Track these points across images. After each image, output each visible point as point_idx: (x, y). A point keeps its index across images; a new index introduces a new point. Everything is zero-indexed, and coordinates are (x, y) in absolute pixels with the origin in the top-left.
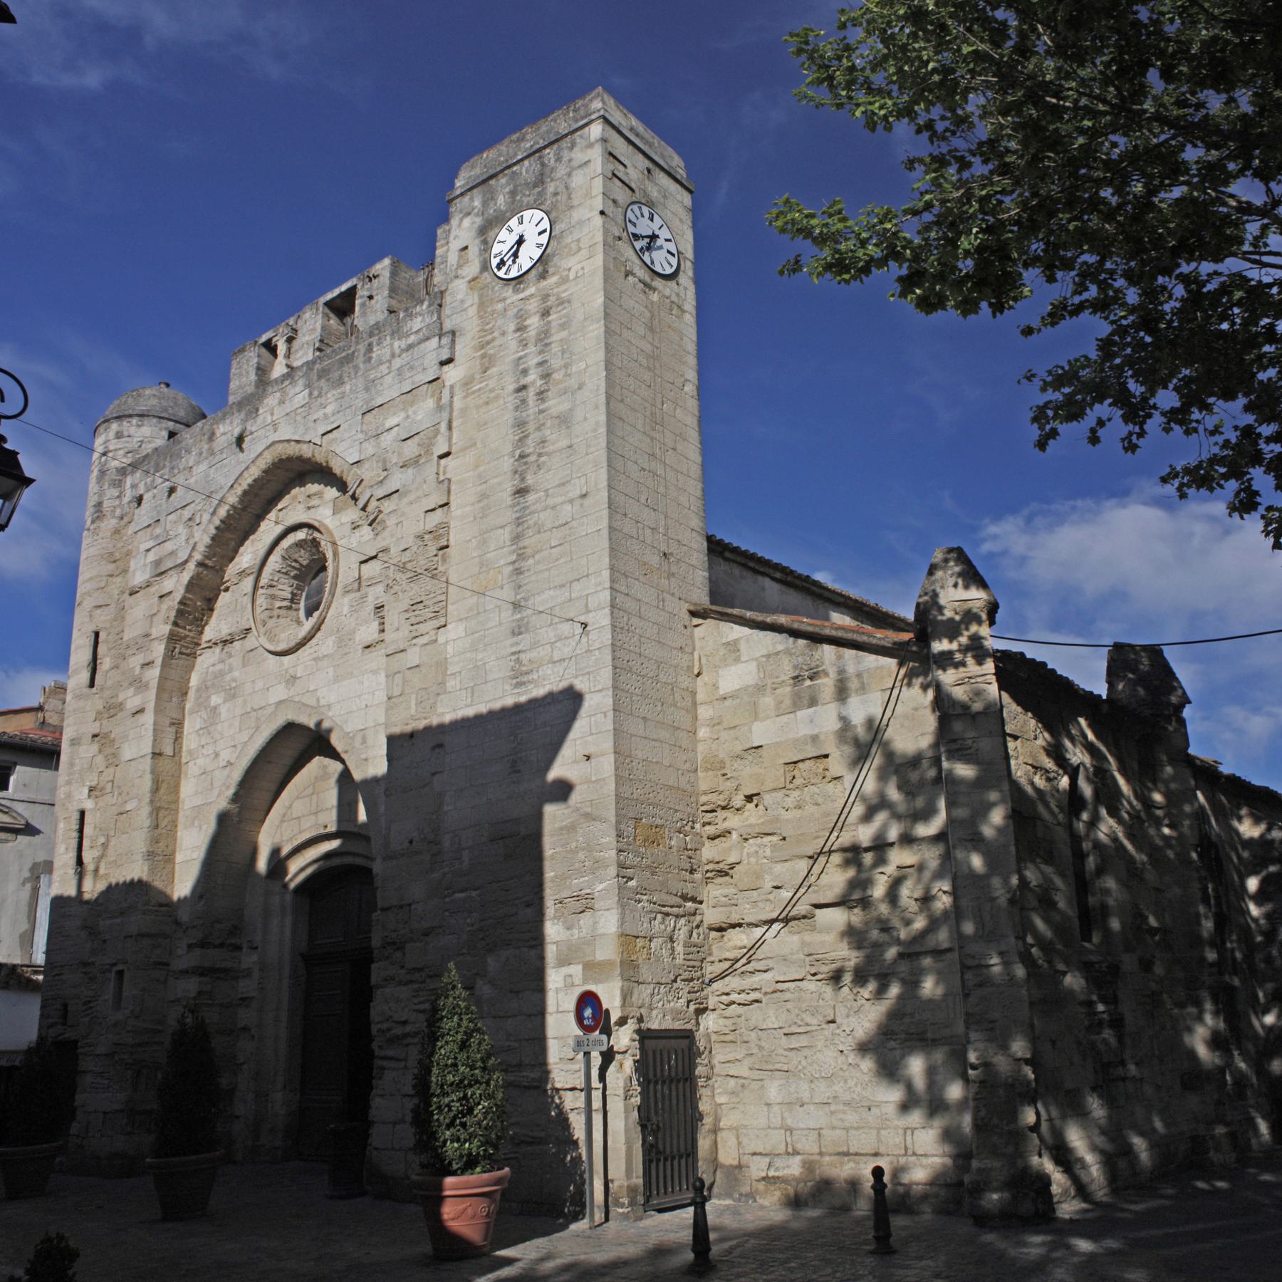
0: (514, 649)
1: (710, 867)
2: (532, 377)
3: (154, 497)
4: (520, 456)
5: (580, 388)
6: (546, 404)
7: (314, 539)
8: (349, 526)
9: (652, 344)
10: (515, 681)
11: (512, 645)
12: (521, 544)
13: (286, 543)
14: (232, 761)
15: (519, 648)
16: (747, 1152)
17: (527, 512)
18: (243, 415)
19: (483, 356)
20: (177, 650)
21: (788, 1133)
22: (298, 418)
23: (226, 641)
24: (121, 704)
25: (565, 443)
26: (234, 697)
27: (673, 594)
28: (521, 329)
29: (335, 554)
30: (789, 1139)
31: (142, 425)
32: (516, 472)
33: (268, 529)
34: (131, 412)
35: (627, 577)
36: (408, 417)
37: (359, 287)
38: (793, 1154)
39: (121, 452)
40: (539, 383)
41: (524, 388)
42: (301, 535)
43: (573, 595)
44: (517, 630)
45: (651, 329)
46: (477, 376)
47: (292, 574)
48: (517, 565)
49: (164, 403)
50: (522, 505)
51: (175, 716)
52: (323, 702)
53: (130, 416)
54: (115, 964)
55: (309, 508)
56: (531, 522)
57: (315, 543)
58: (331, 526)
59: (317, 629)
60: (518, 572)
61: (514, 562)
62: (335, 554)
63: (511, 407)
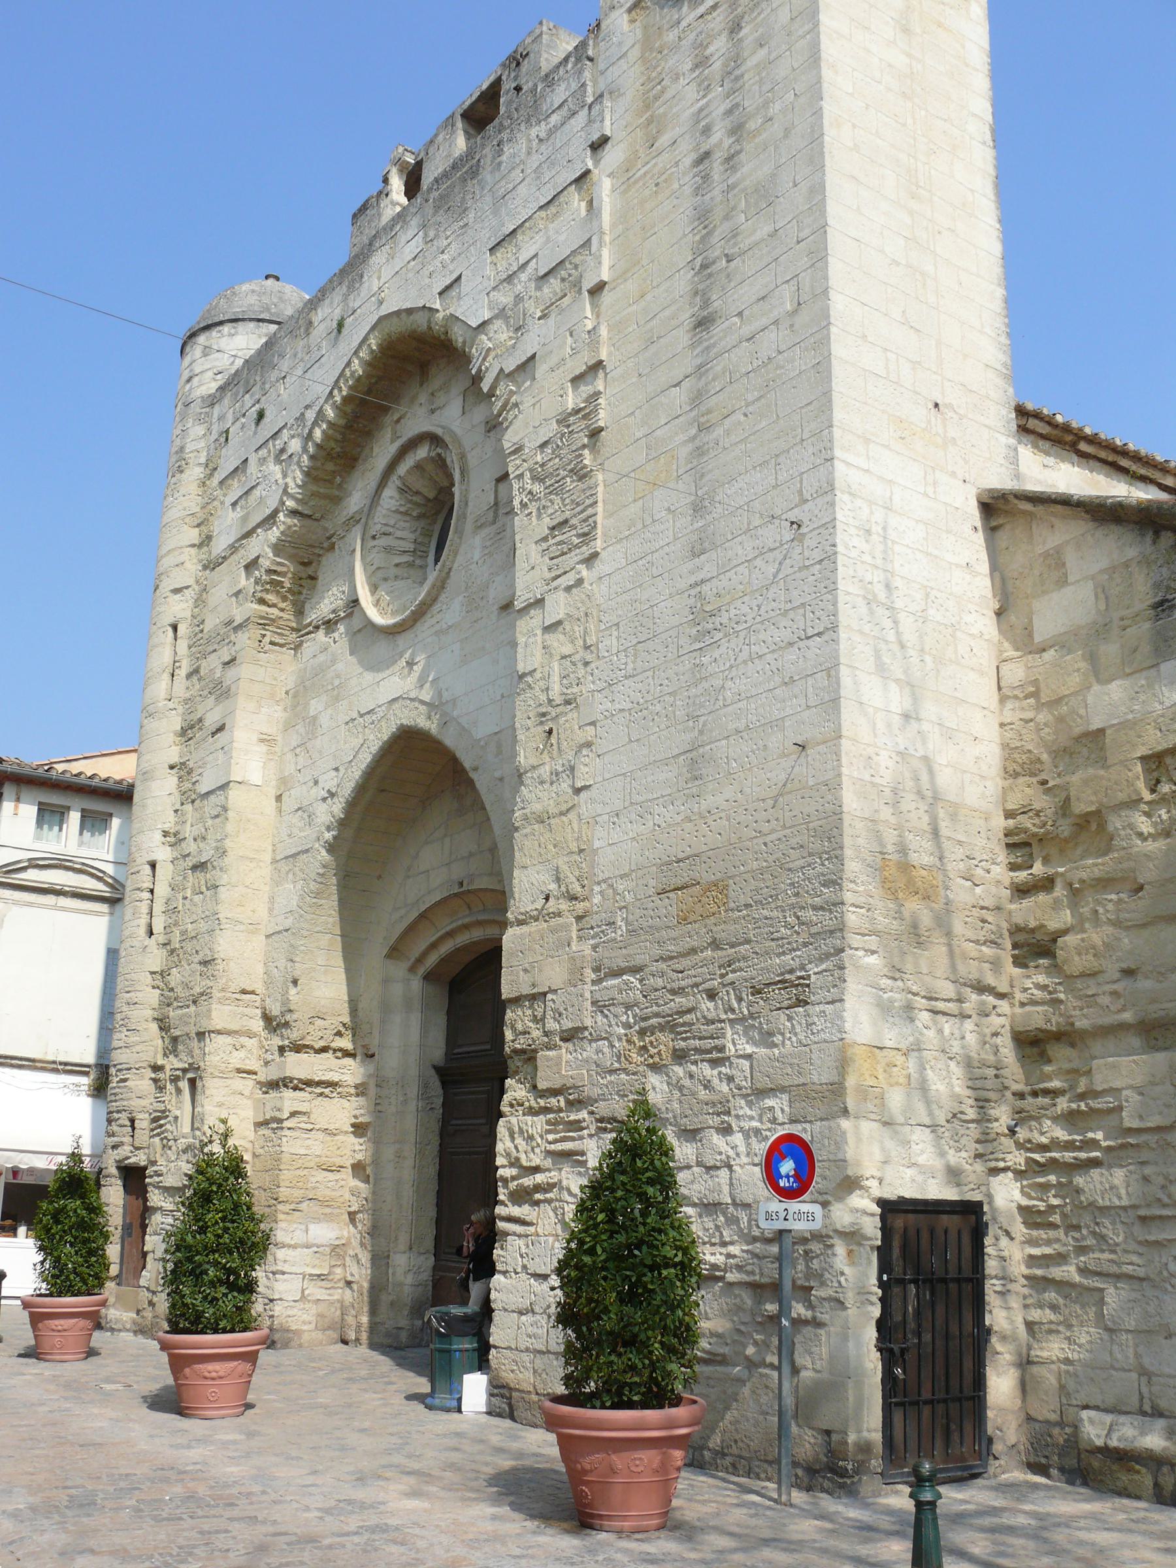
0: (692, 580)
1: (1021, 937)
2: (718, 135)
3: (242, 428)
4: (701, 265)
5: (786, 136)
6: (739, 175)
7: (439, 455)
8: (482, 428)
9: (908, 55)
10: (694, 631)
11: (692, 572)
12: (703, 408)
13: (403, 469)
14: (334, 790)
15: (700, 576)
16: (1074, 1402)
17: (712, 355)
18: (345, 288)
19: (649, 122)
20: (267, 640)
21: (1144, 1380)
22: (410, 275)
23: (329, 621)
24: (200, 720)
25: (768, 229)
26: (337, 699)
27: (953, 474)
28: (702, 63)
29: (463, 472)
30: (1145, 1390)
31: (236, 334)
32: (696, 293)
33: (383, 451)
34: (221, 318)
35: (867, 441)
36: (548, 240)
37: (504, 78)
38: (1152, 1415)
39: (210, 374)
40: (727, 142)
41: (707, 155)
42: (422, 452)
43: (780, 478)
44: (698, 547)
45: (906, 30)
46: (641, 154)
47: (415, 514)
48: (697, 443)
49: (265, 300)
50: (706, 344)
51: (265, 730)
52: (446, 696)
53: (221, 323)
54: (185, 1071)
55: (433, 411)
56: (719, 368)
57: (441, 463)
58: (458, 431)
59: (441, 585)
60: (700, 452)
61: (694, 438)
62: (463, 472)
63: (688, 190)
